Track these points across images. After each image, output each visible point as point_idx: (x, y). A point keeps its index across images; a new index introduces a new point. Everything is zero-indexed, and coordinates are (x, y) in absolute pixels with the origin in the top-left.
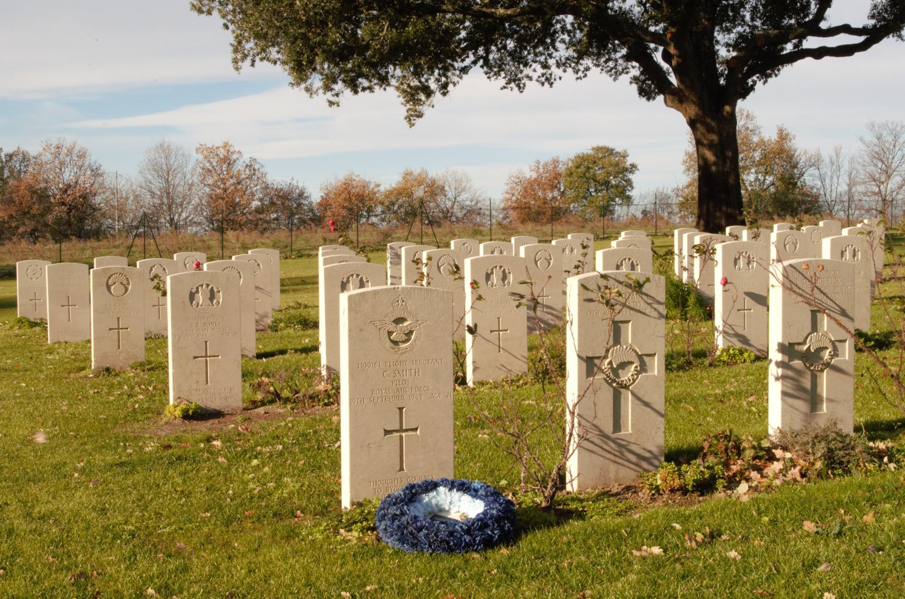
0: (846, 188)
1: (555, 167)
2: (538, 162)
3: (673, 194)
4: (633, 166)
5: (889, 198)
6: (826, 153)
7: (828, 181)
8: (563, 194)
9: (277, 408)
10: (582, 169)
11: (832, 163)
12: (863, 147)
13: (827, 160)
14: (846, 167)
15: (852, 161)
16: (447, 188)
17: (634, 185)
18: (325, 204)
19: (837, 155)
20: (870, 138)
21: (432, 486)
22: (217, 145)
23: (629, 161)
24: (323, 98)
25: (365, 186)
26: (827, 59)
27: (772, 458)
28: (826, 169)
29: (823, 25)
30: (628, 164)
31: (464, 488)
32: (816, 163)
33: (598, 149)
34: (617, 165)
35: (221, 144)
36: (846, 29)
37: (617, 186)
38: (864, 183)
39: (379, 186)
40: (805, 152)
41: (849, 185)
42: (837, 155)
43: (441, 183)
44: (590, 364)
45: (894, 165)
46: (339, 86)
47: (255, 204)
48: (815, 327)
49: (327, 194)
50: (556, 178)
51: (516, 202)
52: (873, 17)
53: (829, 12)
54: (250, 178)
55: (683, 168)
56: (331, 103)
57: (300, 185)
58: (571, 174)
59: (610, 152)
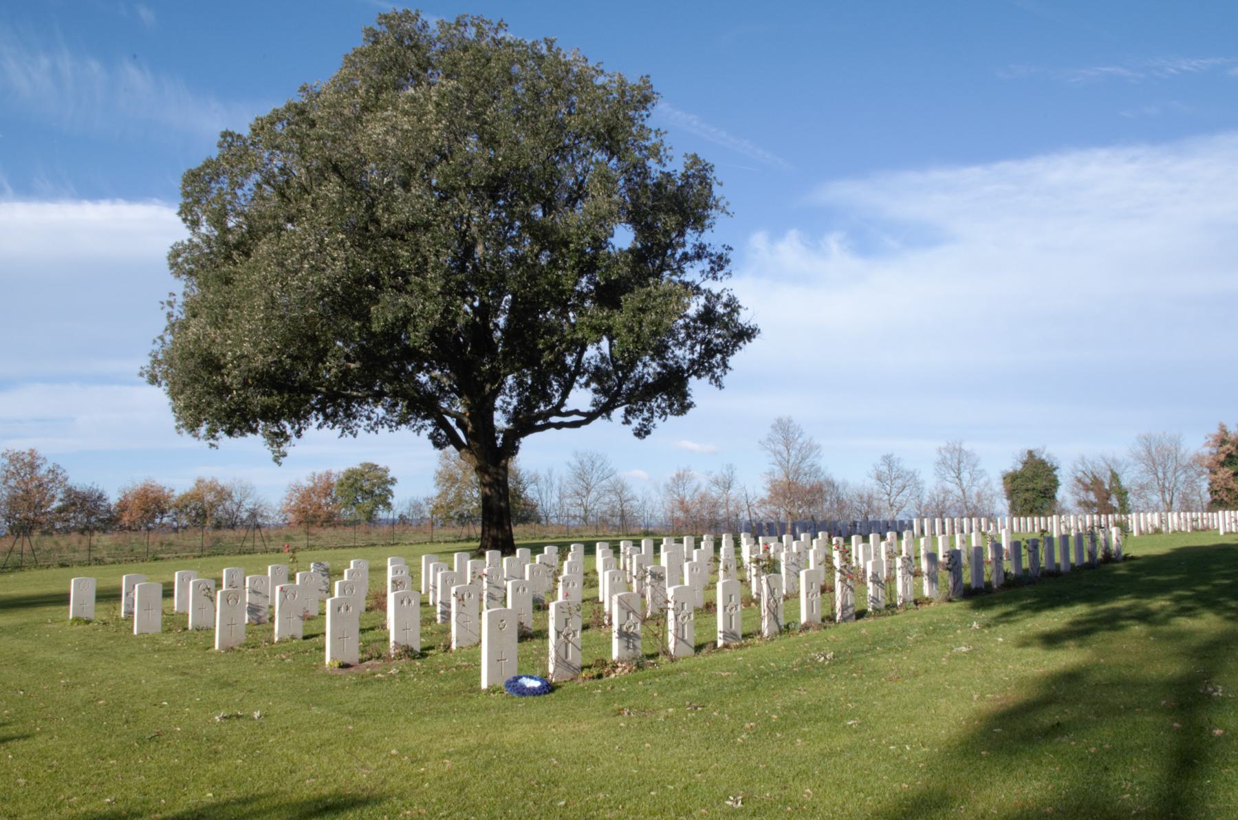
0: (557, 500)
1: (328, 479)
2: (314, 474)
3: (424, 503)
4: (393, 479)
5: (589, 508)
6: (543, 473)
7: (544, 495)
8: (334, 501)
9: (373, 661)
10: (351, 481)
11: (547, 481)
12: (569, 469)
13: (543, 479)
14: (557, 483)
15: (561, 479)
16: (234, 494)
17: (394, 494)
18: (123, 506)
19: (550, 474)
20: (574, 462)
21: (520, 677)
22: (23, 450)
23: (390, 475)
24: (204, 444)
25: (162, 489)
26: (564, 430)
27: (617, 667)
28: (543, 486)
29: (563, 410)
30: (389, 478)
31: (531, 677)
32: (535, 480)
33: (365, 465)
34: (380, 478)
35: (27, 452)
36: (576, 412)
37: (380, 495)
38: (571, 497)
39: (173, 491)
40: (528, 472)
41: (560, 498)
42: (550, 474)
43: (229, 490)
44: (558, 633)
45: (592, 484)
46: (221, 434)
47: (56, 504)
48: (628, 618)
49: (125, 497)
50: (328, 488)
51: (294, 506)
52: (593, 405)
53: (567, 401)
54: (53, 481)
55: (434, 483)
56: (212, 445)
57: (100, 489)
58: (342, 485)
59: (374, 467)
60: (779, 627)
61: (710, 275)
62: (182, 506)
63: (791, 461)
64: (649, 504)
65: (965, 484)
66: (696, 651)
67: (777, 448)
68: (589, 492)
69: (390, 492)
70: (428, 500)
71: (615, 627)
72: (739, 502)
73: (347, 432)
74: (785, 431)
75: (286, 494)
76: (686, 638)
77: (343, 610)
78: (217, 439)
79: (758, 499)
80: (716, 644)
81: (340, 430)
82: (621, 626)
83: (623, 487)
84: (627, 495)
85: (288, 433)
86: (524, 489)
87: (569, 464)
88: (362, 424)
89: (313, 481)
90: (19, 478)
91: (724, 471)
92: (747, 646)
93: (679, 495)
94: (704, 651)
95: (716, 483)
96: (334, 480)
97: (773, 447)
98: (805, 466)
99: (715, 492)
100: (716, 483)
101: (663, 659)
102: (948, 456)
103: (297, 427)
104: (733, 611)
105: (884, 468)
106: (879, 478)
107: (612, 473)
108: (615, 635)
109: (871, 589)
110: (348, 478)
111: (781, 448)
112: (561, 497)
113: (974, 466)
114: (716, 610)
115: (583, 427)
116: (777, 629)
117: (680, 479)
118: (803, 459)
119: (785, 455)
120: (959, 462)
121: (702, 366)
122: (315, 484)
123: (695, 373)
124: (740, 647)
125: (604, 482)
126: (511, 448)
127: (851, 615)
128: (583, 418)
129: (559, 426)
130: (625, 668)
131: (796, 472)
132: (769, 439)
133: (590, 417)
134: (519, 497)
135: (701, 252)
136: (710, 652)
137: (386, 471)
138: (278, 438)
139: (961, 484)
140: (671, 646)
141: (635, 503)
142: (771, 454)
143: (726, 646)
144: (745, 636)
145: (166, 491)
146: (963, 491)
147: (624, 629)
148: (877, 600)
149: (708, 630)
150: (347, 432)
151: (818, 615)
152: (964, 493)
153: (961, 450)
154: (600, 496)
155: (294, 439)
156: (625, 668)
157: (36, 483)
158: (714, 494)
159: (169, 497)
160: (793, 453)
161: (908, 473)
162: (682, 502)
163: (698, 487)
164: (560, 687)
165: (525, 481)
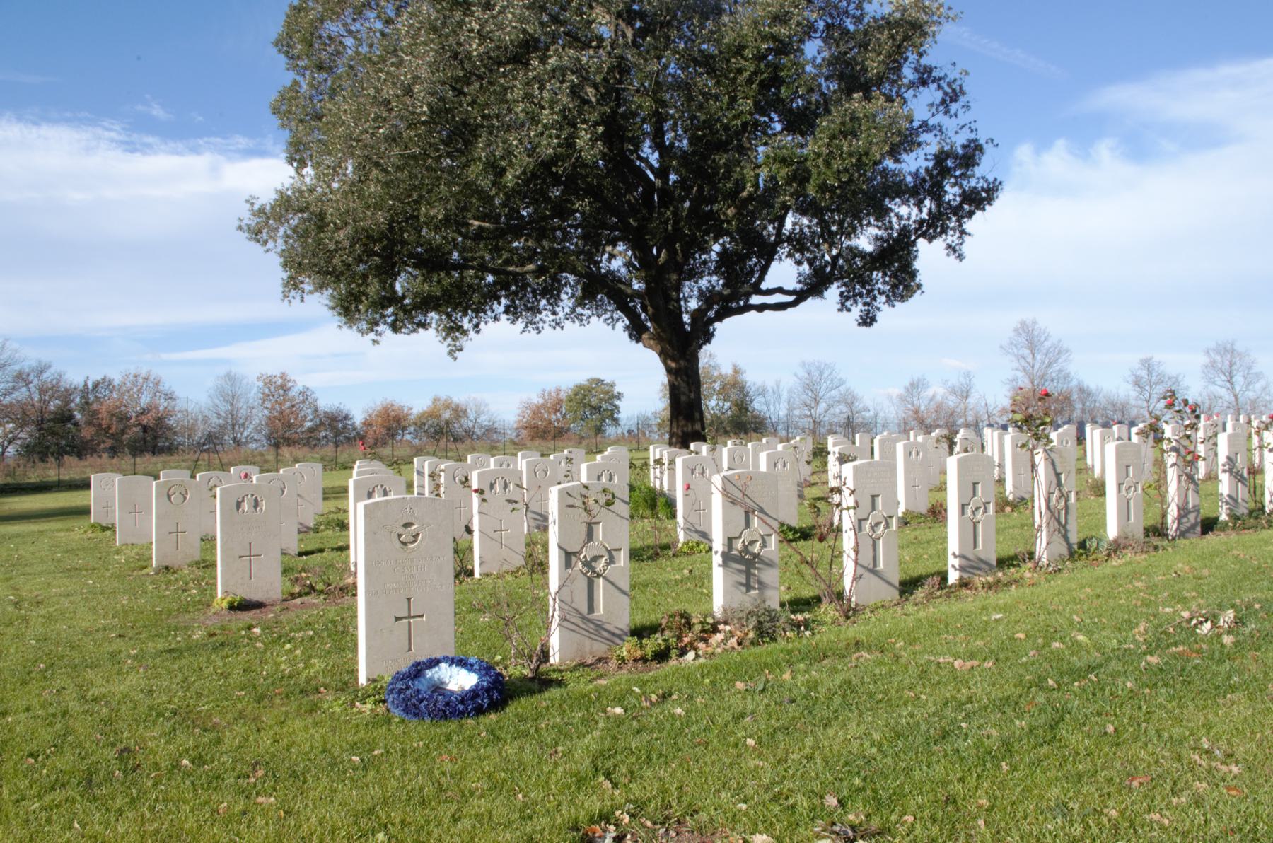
2: (544, 391)
6: (770, 384)
8: (564, 416)
9: (312, 599)
14: (785, 395)
18: (368, 424)
20: (802, 373)
21: (434, 663)
23: (617, 389)
26: (767, 312)
32: (763, 393)
34: (607, 392)
36: (780, 290)
38: (799, 408)
42: (778, 386)
43: (464, 407)
44: (568, 557)
45: (821, 394)
48: (748, 525)
52: (800, 282)
53: (767, 277)
54: (303, 402)
57: (346, 408)
58: (571, 400)
59: (599, 382)
60: (1070, 546)
61: (941, 108)
62: (420, 424)
63: (1036, 367)
64: (881, 414)
65: (1237, 388)
66: (902, 593)
67: (1020, 352)
68: (818, 403)
69: (617, 407)
70: (654, 413)
71: (718, 545)
72: (978, 412)
73: (530, 327)
74: (1030, 338)
75: (519, 411)
76: (881, 566)
77: (246, 506)
78: (380, 335)
79: (998, 409)
80: (944, 577)
81: (523, 325)
82: (730, 541)
83: (854, 398)
84: (858, 406)
85: (465, 327)
86: (752, 402)
87: (796, 375)
88: (547, 319)
89: (544, 398)
90: (273, 400)
91: (962, 379)
92: (1009, 584)
93: (913, 405)
94: (920, 594)
95: (953, 392)
96: (563, 396)
97: (1015, 351)
98: (1053, 372)
99: (952, 401)
100: (953, 392)
101: (828, 611)
102: (1218, 358)
103: (475, 321)
104: (980, 515)
105: (1143, 373)
106: (1137, 383)
107: (842, 382)
108: (717, 559)
109: (1225, 485)
110: (576, 394)
111: (1027, 352)
112: (790, 409)
113: (1250, 368)
114: (945, 518)
115: (790, 310)
116: (1065, 551)
117: (915, 387)
118: (1050, 365)
119: (1030, 359)
120: (1231, 365)
121: (933, 227)
122: (545, 400)
123: (924, 235)
124: (994, 586)
125: (834, 393)
126: (702, 332)
127: (1193, 527)
128: (791, 298)
129: (761, 308)
130: (732, 634)
131: (1042, 377)
132: (1012, 343)
133: (801, 296)
134: (747, 409)
135: (925, 77)
136: (930, 597)
137: (612, 385)
138: (453, 330)
139: (1233, 388)
140: (847, 582)
141: (867, 414)
142: (1014, 359)
143: (964, 584)
144: (1003, 563)
145: (406, 410)
146: (1236, 397)
147: (739, 545)
148: (1236, 501)
149: (932, 550)
150: (530, 327)
151: (1137, 528)
152: (1236, 397)
153: (1233, 351)
154: (830, 407)
155: (472, 334)
156: (732, 634)
157: (288, 404)
158: (951, 403)
159: (407, 415)
160: (1038, 357)
161: (1169, 378)
162: (916, 412)
163: (934, 396)
164: (560, 683)
165: (751, 393)
